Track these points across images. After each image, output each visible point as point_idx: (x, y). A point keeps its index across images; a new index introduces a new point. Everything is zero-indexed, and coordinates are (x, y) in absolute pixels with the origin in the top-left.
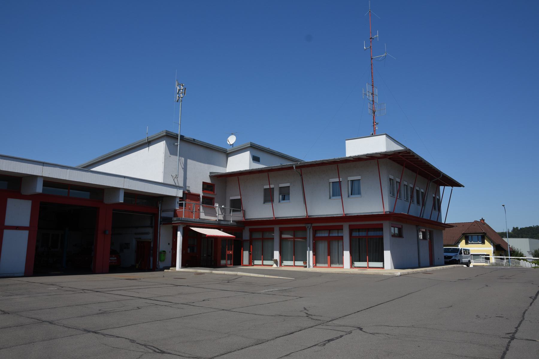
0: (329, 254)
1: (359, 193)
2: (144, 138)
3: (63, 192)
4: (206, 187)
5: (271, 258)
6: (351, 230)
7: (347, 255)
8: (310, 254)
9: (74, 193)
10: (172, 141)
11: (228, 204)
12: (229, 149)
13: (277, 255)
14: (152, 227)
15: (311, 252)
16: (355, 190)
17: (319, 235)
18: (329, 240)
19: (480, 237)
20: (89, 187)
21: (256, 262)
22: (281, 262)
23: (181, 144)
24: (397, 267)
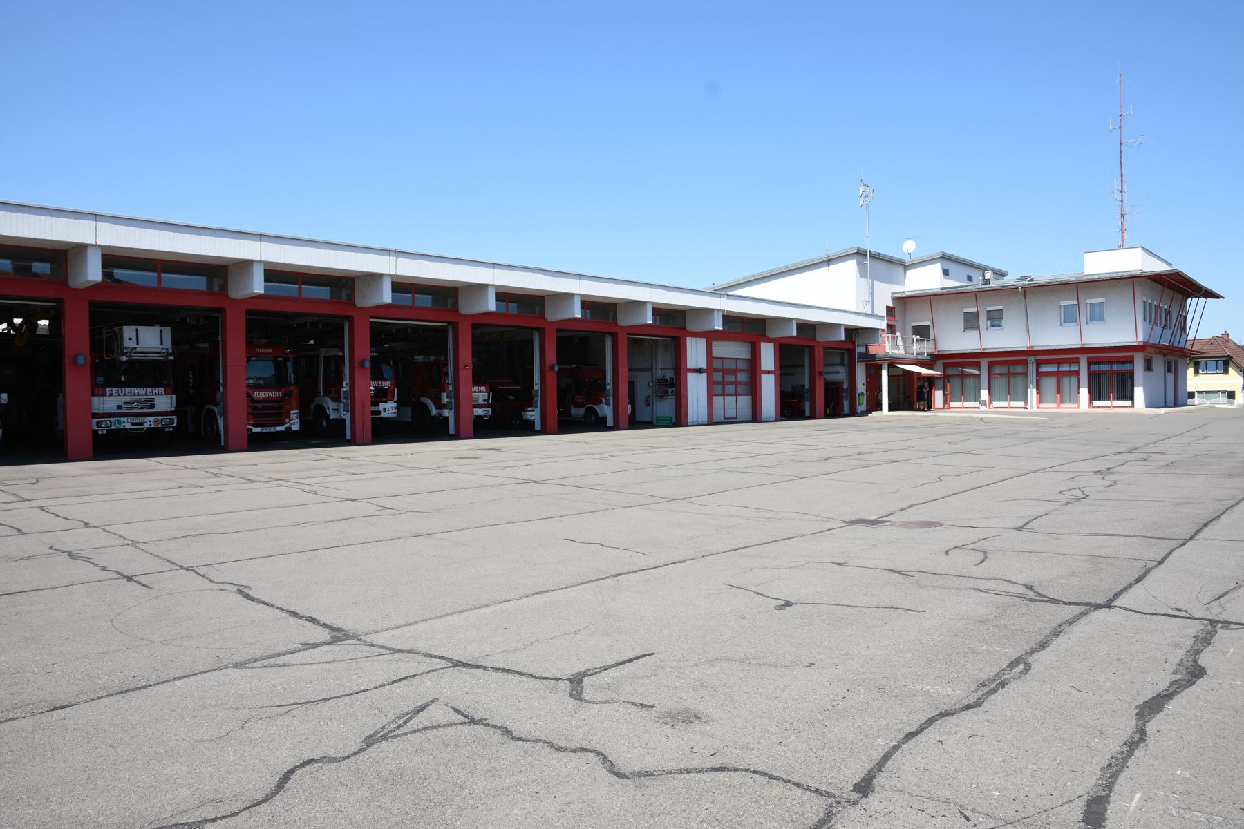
0: (1058, 392)
1: (1101, 319)
2: (821, 254)
3: (146, 278)
4: (890, 311)
5: (977, 398)
6: (1090, 364)
7: (1084, 392)
8: (1032, 392)
9: (172, 280)
10: (861, 258)
11: (910, 331)
12: (908, 261)
13: (984, 394)
14: (842, 364)
15: (1034, 390)
16: (1097, 315)
17: (1043, 369)
18: (1059, 375)
19: (1220, 363)
20: (159, 261)
21: (952, 404)
22: (990, 403)
23: (876, 262)
24: (1149, 405)
